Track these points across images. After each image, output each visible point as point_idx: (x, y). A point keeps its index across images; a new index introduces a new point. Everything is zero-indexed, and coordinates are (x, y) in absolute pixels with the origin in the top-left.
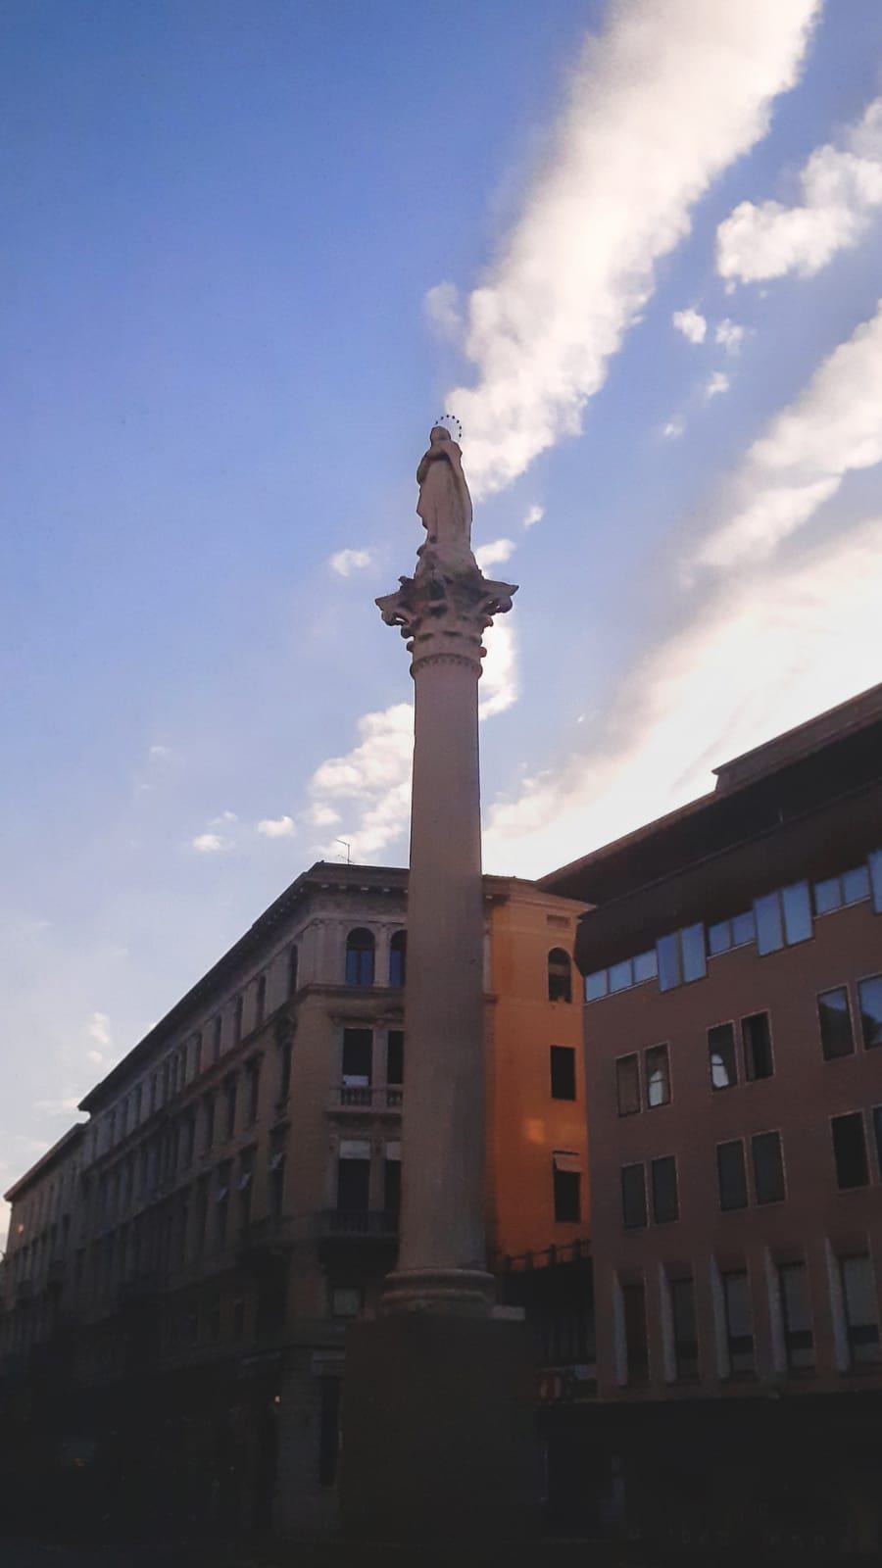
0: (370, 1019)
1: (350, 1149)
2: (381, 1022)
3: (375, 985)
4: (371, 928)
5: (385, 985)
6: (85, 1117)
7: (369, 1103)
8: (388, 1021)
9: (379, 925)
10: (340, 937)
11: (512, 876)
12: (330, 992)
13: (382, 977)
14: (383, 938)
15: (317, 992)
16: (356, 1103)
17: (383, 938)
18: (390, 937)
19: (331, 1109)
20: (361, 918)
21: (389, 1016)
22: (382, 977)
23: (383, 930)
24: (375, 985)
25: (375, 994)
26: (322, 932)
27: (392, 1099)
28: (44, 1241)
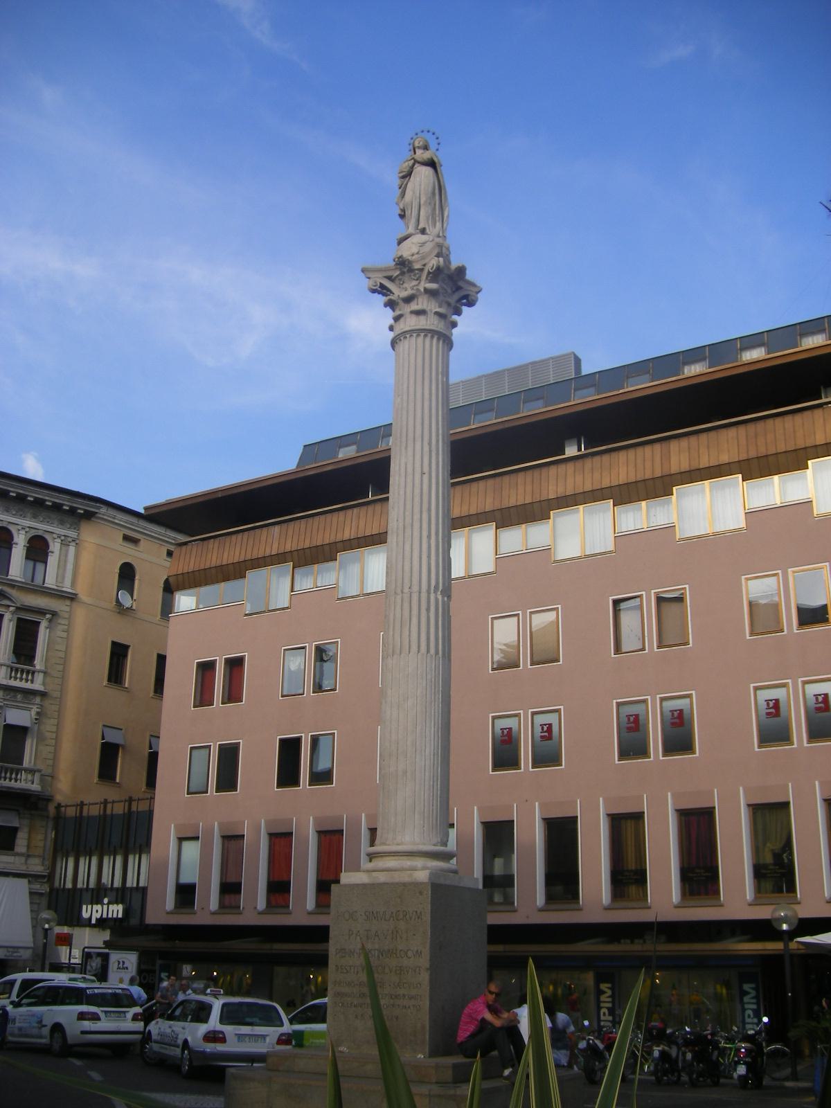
9: (20, 527)
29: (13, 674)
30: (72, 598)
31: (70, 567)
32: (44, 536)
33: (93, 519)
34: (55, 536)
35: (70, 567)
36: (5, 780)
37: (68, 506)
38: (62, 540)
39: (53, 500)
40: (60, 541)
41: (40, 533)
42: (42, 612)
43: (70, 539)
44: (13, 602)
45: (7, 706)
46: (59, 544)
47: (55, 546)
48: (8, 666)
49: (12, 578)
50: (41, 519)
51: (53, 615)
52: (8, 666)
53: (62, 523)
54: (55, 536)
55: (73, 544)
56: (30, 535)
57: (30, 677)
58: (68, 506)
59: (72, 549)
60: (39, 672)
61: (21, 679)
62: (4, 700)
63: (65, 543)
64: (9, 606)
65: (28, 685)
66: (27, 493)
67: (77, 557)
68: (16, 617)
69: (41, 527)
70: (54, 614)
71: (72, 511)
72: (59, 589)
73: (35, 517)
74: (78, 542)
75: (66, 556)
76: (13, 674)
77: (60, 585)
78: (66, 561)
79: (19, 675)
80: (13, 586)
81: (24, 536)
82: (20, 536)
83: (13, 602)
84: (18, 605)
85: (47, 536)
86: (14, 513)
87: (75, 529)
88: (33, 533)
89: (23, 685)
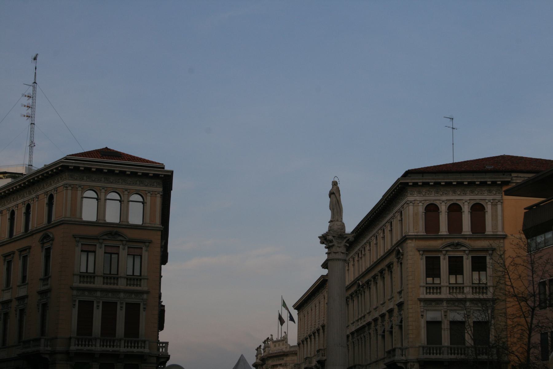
0: (440, 251)
1: (431, 315)
2: (444, 252)
3: (486, 233)
4: (437, 203)
5: (445, 233)
6: (325, 272)
7: (117, 284)
8: (447, 251)
9: (464, 201)
10: (421, 209)
11: (104, 147)
12: (417, 238)
13: (444, 229)
14: (443, 208)
15: (412, 239)
16: (87, 282)
17: (443, 208)
18: (470, 208)
19: (422, 296)
20: (432, 197)
21: (105, 237)
22: (444, 229)
23: (466, 203)
24: (486, 233)
25: (442, 238)
26: (411, 207)
27: (129, 282)
28: (311, 339)
29: (428, 291)
30: (504, 237)
31: (500, 218)
32: (480, 202)
33: (510, 184)
34: (487, 201)
35: (500, 218)
36: (128, 348)
37: (490, 181)
38: (492, 203)
39: (479, 180)
40: (490, 204)
41: (478, 201)
42: (485, 250)
43: (497, 201)
44: (468, 248)
45: (427, 310)
46: (491, 205)
47: (489, 208)
48: (470, 287)
49: (465, 233)
50: (494, 192)
51: (493, 251)
52: (470, 287)
53: (490, 191)
54: (487, 201)
55: (499, 203)
56: (448, 205)
57: (438, 291)
58: (490, 181)
59: (499, 207)
60: (466, 287)
61: (433, 293)
62: (448, 307)
63: (494, 204)
64: (465, 251)
65: (92, 285)
66: (463, 180)
67: (503, 211)
68: (470, 256)
69: (477, 197)
70: (494, 250)
71: (494, 183)
72: (495, 233)
73: (472, 192)
74: (502, 201)
75: (496, 211)
76: (428, 291)
77: (495, 231)
78: (497, 216)
79: (431, 291)
80: (466, 238)
81: (444, 206)
82: (465, 206)
83: (125, 238)
84: (470, 249)
85: (482, 203)
86: (459, 193)
87: (499, 193)
88: (473, 203)
89: (112, 287)
